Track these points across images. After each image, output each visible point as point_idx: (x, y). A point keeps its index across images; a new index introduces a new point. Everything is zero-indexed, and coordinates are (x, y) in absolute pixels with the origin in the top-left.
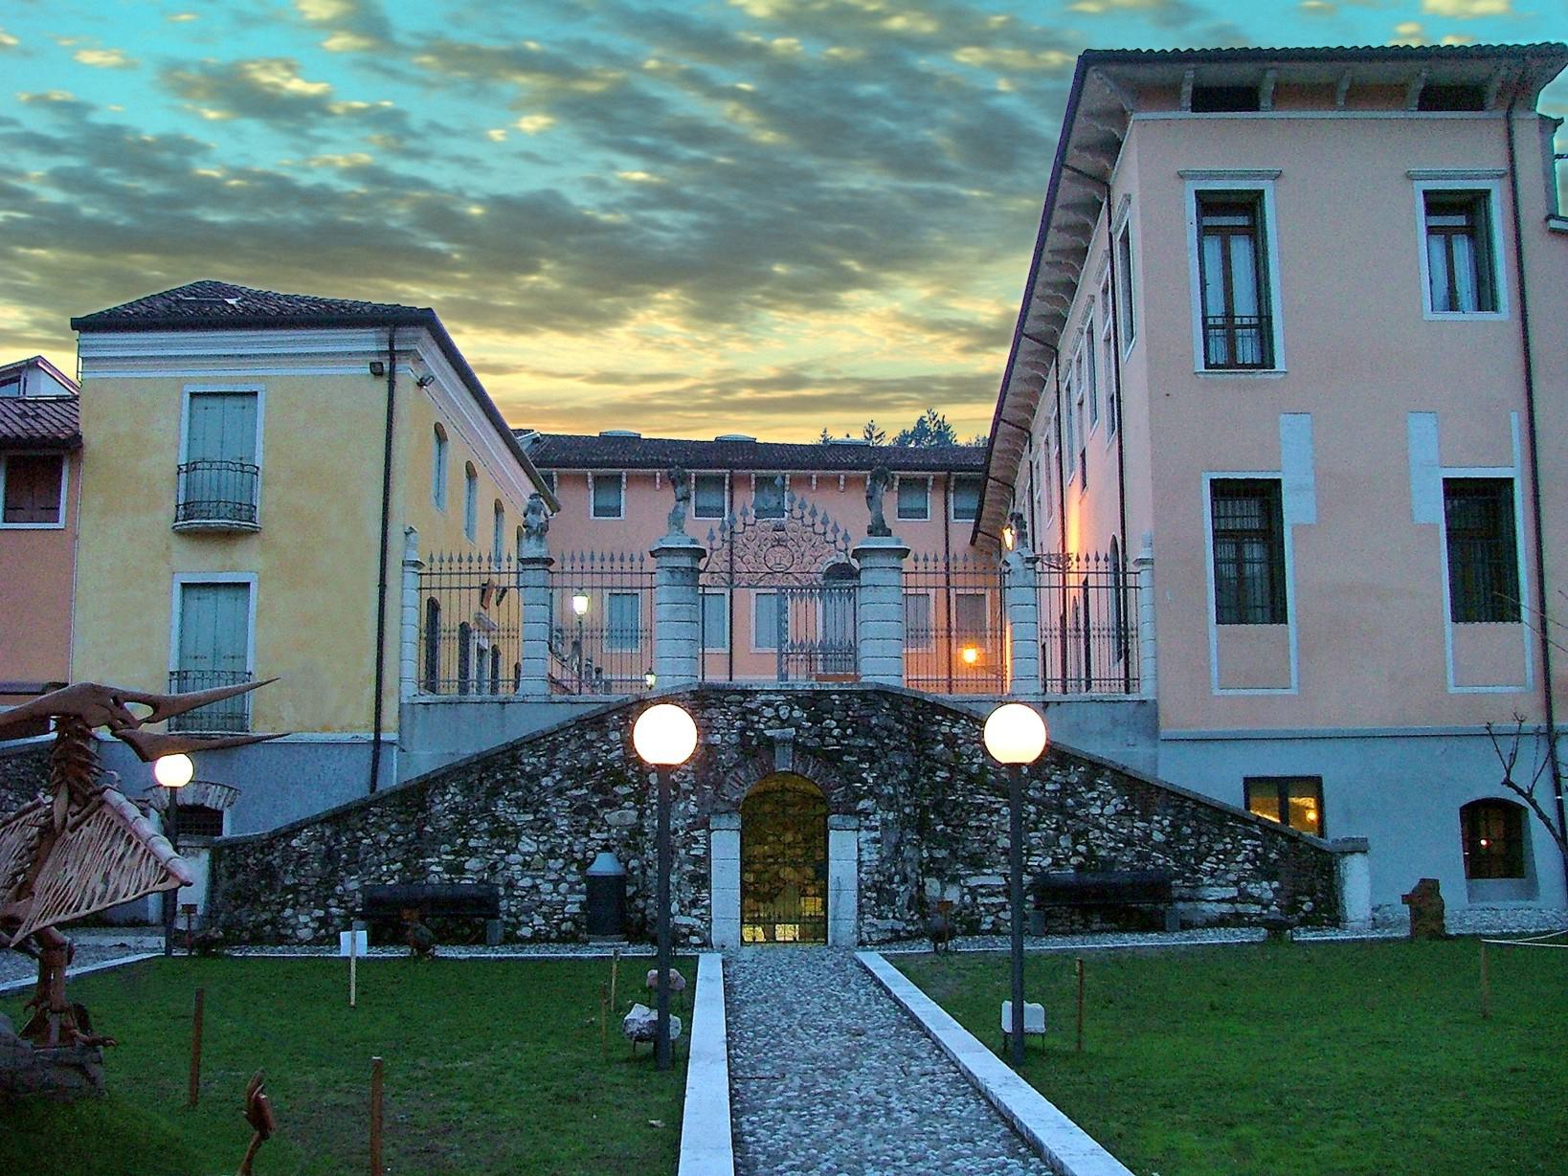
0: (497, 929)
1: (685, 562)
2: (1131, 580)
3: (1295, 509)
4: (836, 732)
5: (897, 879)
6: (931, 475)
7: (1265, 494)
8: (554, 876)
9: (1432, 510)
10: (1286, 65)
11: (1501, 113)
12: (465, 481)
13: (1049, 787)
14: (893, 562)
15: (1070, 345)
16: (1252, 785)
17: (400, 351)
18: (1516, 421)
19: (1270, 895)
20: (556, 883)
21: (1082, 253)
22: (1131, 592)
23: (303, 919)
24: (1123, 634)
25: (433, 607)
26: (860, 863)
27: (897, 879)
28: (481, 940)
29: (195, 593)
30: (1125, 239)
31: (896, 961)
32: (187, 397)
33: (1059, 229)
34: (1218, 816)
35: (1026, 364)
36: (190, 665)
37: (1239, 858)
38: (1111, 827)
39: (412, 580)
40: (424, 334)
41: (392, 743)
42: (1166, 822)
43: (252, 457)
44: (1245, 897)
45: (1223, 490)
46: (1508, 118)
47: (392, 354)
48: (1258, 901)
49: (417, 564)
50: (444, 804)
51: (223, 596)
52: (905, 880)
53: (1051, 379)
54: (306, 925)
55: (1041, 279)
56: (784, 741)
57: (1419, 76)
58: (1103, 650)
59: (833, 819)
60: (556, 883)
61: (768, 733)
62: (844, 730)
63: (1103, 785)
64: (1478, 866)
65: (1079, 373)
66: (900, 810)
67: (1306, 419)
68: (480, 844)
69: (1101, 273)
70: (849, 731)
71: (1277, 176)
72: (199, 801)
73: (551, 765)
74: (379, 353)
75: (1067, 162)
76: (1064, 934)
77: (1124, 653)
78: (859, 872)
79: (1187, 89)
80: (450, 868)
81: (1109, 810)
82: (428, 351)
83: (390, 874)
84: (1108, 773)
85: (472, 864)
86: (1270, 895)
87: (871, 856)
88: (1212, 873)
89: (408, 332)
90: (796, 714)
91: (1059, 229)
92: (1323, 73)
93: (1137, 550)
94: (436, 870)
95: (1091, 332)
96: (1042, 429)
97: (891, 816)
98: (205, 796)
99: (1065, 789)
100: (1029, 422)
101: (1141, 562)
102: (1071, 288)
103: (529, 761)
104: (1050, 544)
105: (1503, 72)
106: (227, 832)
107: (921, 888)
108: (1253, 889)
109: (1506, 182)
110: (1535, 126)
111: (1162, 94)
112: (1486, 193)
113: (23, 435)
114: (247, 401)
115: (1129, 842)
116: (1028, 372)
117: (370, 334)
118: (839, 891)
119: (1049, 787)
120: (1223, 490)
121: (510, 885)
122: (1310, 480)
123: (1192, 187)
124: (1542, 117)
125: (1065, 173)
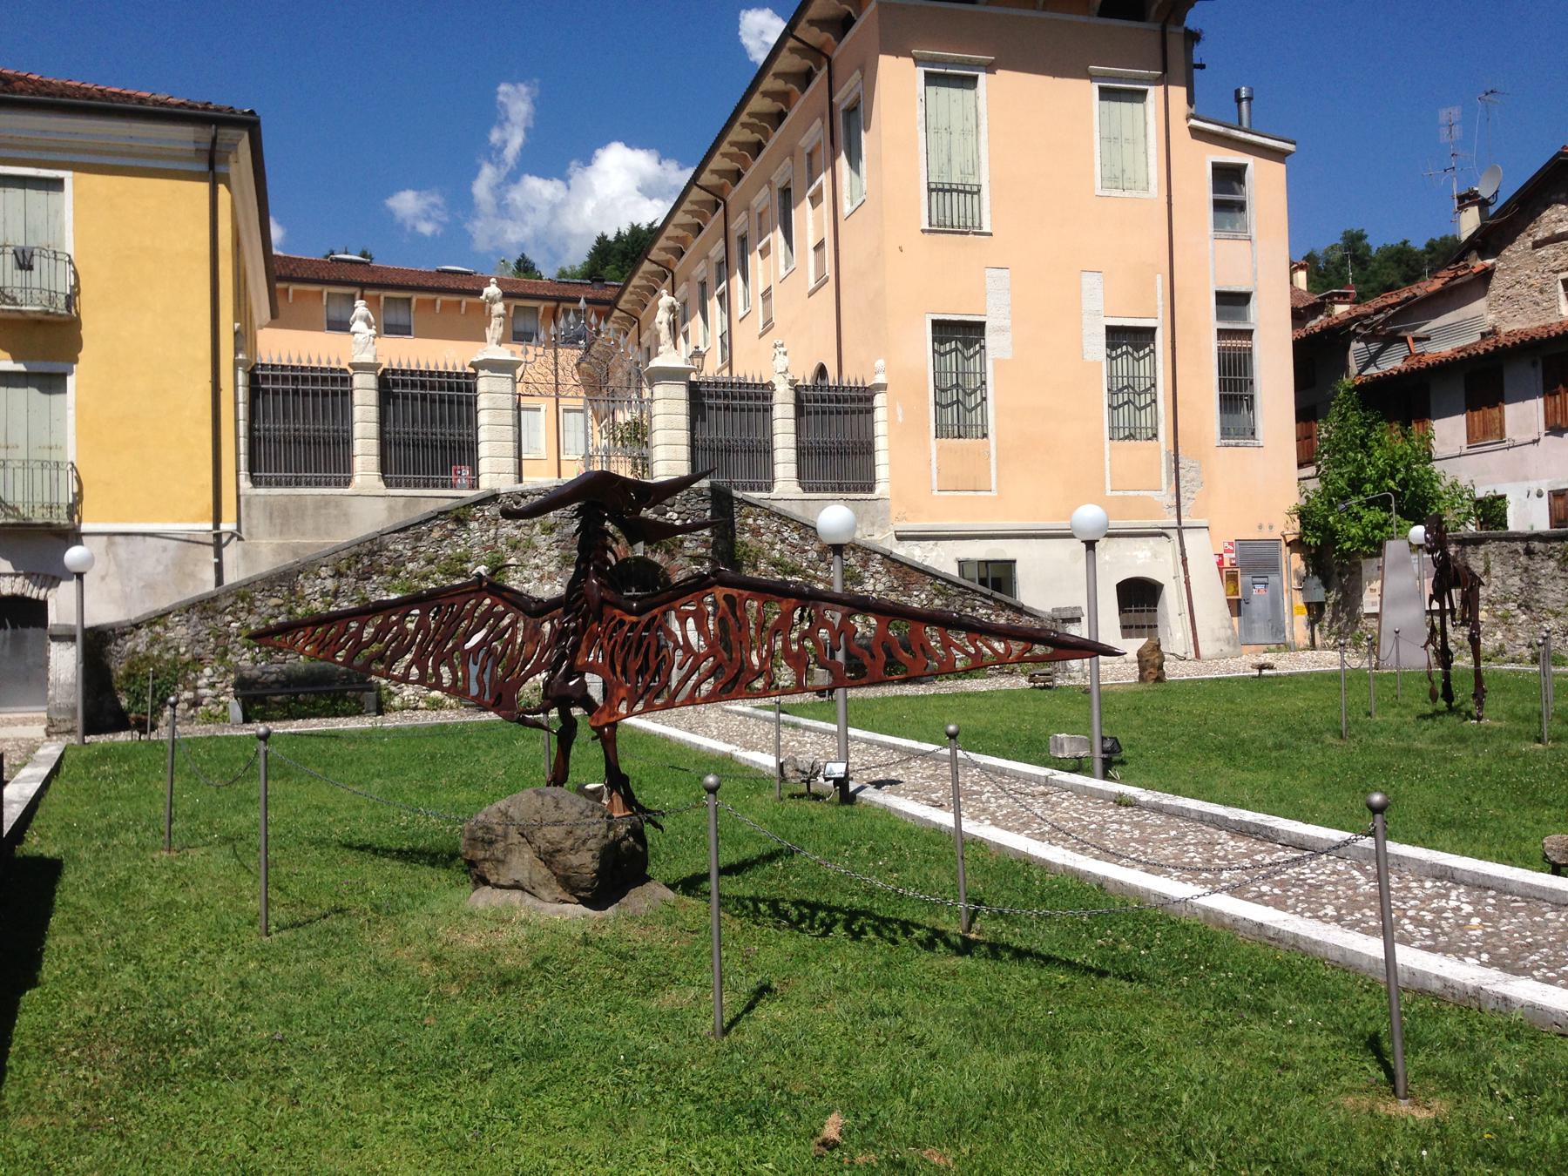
6: (542, 306)
11: (1157, 27)
18: (1161, 282)
122: (1007, 323)
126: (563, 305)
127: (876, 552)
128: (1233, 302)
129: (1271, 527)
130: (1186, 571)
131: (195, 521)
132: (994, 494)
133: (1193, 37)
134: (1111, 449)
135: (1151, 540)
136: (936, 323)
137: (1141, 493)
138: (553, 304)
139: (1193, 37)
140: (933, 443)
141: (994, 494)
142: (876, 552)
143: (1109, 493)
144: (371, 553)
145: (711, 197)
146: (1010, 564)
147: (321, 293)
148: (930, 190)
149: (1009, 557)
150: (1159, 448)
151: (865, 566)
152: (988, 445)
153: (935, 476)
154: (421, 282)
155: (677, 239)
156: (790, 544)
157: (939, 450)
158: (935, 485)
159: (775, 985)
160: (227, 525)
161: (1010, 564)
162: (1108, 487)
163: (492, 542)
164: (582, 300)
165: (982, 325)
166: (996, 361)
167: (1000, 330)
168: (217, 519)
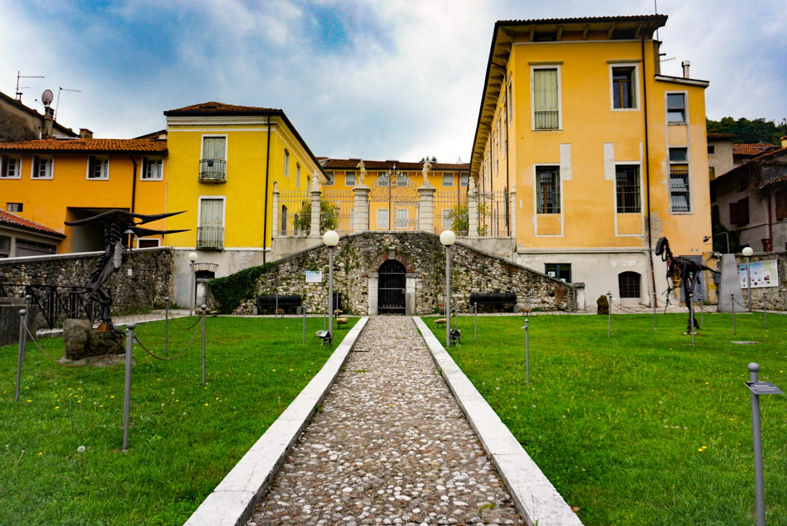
0: (299, 309)
1: (364, 193)
5: (428, 294)
6: (454, 172)
7: (553, 171)
8: (319, 293)
9: (611, 175)
10: (565, 25)
11: (640, 40)
12: (296, 168)
13: (479, 265)
14: (430, 193)
16: (549, 267)
17: (272, 124)
18: (641, 145)
19: (552, 301)
20: (320, 295)
21: (498, 94)
26: (416, 289)
27: (428, 294)
28: (295, 313)
29: (205, 202)
30: (510, 87)
31: (424, 320)
32: (202, 138)
33: (491, 85)
35: (481, 133)
36: (204, 225)
37: (542, 289)
38: (499, 278)
39: (275, 198)
40: (280, 118)
41: (269, 251)
42: (517, 277)
43: (224, 158)
45: (540, 170)
46: (643, 42)
48: (548, 303)
49: (278, 193)
50: (285, 268)
51: (215, 202)
53: (489, 138)
55: (485, 103)
57: (613, 27)
60: (320, 295)
62: (412, 246)
63: (497, 265)
64: (624, 294)
65: (501, 139)
66: (430, 272)
67: (569, 145)
70: (413, 246)
71: (561, 63)
72: (207, 269)
73: (318, 257)
76: (17, 117)
79: (532, 34)
80: (286, 290)
81: (499, 273)
82: (281, 124)
84: (498, 261)
86: (552, 301)
90: (396, 241)
91: (491, 85)
92: (579, 27)
93: (512, 190)
95: (500, 120)
96: (487, 155)
98: (209, 267)
100: (483, 153)
101: (513, 193)
102: (495, 106)
103: (312, 256)
104: (488, 189)
105: (641, 25)
106: (216, 277)
108: (546, 299)
109: (641, 64)
110: (652, 44)
111: (524, 36)
112: (634, 68)
113: (149, 150)
114: (222, 140)
116: (483, 135)
117: (261, 118)
120: (540, 170)
122: (570, 166)
124: (654, 41)
125: (492, 65)
127: (497, 259)
128: (678, 153)
129: (697, 250)
130: (652, 269)
132: (562, 236)
133: (658, 43)
134: (618, 217)
135: (636, 256)
137: (632, 235)
138: (458, 171)
139: (658, 43)
140: (536, 216)
141: (32, 177)
142: (497, 259)
146: (569, 265)
147: (343, 172)
148: (536, 113)
149: (568, 262)
150: (641, 216)
151: (492, 264)
152: (560, 217)
154: (442, 167)
155: (482, 143)
156: (461, 256)
157: (538, 219)
161: (569, 265)
164: (40, 138)
165: (558, 168)
167: (566, 169)
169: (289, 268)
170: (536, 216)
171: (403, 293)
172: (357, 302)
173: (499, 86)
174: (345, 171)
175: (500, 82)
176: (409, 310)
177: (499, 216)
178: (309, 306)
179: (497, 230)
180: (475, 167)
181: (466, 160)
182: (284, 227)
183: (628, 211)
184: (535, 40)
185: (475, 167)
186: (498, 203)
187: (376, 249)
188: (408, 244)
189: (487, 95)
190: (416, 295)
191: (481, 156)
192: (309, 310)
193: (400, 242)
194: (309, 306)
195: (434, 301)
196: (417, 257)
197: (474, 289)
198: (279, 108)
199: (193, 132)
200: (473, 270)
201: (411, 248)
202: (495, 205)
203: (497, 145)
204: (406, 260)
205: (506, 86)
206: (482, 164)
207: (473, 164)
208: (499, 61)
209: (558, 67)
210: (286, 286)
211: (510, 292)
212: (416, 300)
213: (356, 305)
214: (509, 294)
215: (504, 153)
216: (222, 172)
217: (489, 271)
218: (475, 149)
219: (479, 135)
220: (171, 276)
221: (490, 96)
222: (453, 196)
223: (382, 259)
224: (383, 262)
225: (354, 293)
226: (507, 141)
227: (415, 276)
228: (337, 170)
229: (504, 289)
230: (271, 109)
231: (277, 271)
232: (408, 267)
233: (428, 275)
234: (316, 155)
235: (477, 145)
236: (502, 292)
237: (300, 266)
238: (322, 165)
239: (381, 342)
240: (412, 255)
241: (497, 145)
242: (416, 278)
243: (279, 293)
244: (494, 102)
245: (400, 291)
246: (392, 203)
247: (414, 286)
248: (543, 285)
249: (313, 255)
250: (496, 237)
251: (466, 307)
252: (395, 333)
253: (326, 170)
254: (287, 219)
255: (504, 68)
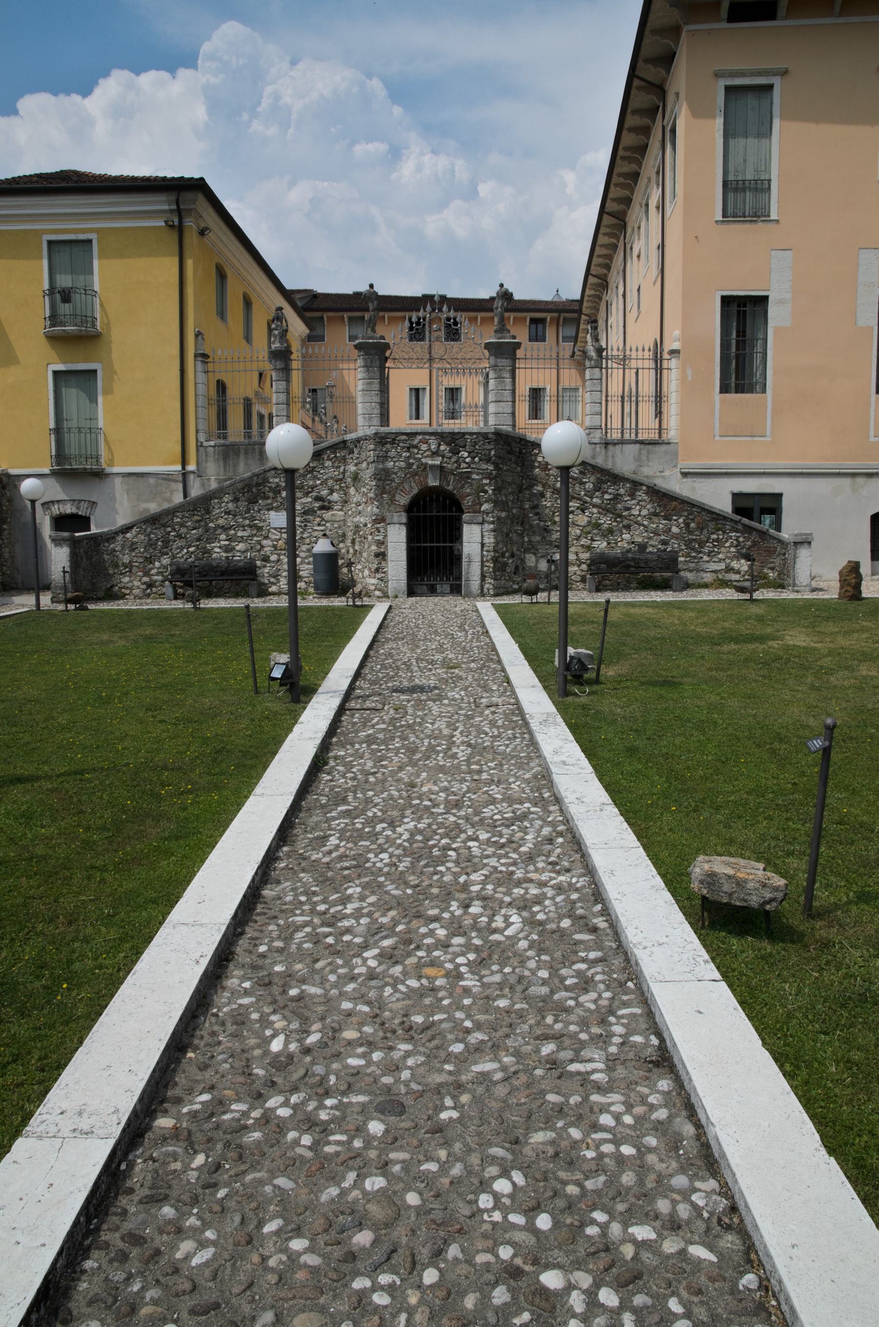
2: (665, 364)
3: (777, 316)
4: (468, 460)
6: (548, 316)
13: (607, 496)
15: (635, 215)
22: (665, 372)
23: (136, 583)
24: (659, 399)
25: (221, 387)
26: (483, 545)
27: (507, 555)
30: (673, 131)
32: (45, 245)
34: (716, 517)
35: (605, 234)
37: (727, 544)
38: (646, 523)
41: (193, 472)
42: (681, 520)
44: (729, 569)
47: (179, 212)
52: (513, 556)
54: (138, 587)
56: (432, 466)
58: (647, 410)
59: (465, 517)
61: (424, 460)
62: (473, 458)
63: (641, 494)
65: (647, 244)
68: (245, 534)
69: (656, 158)
70: (477, 459)
71: (784, 73)
74: (171, 211)
75: (637, 73)
77: (659, 413)
78: (482, 550)
80: (227, 549)
81: (644, 512)
83: (185, 554)
85: (241, 547)
87: (490, 540)
88: (709, 554)
89: (188, 195)
93: (671, 344)
94: (217, 553)
96: (614, 277)
97: (503, 514)
99: (617, 498)
100: (606, 275)
107: (523, 561)
108: (735, 564)
115: (656, 533)
118: (470, 562)
119: (607, 496)
121: (266, 559)
123: (722, 83)
125: (636, 82)
126: (563, 315)
131: (165, 464)
132: (768, 439)
136: (723, 298)
138: (556, 315)
141: (768, 439)
143: (872, 439)
144: (258, 485)
145: (618, 221)
146: (778, 496)
147: (343, 318)
149: (777, 490)
151: (632, 495)
153: (717, 425)
158: (717, 431)
159: (829, 721)
160: (191, 467)
161: (778, 496)
162: (872, 433)
163: (341, 476)
166: (776, 329)
167: (782, 302)
168: (184, 463)
169: (231, 506)
170: (717, 397)
171: (456, 553)
172: (366, 572)
173: (646, 131)
174: (346, 315)
175: (649, 121)
176: (468, 587)
177: (640, 399)
178: (272, 580)
179: (633, 426)
180: (590, 304)
181: (572, 290)
182: (222, 423)
183: (740, 389)
184: (734, 17)
185: (590, 304)
186: (637, 374)
187: (403, 464)
188: (466, 454)
189: (621, 153)
190: (482, 556)
191: (604, 284)
192: (273, 589)
193: (450, 451)
194: (272, 580)
195: (517, 567)
196: (485, 481)
197: (595, 544)
198: (197, 176)
199: (24, 231)
200: (594, 506)
201: (473, 462)
202: (631, 375)
203: (639, 256)
204: (463, 487)
205: (663, 127)
206: (605, 298)
207: (586, 298)
208: (650, 73)
209: (776, 81)
210: (227, 543)
211: (665, 550)
212: (482, 566)
213: (365, 578)
214: (663, 555)
215: (655, 271)
216: (89, 314)
217: (629, 509)
218: (592, 267)
219: (602, 240)
220: (5, 526)
221: (628, 154)
222: (548, 356)
223: (413, 485)
224: (415, 491)
225: (361, 553)
226: (662, 247)
227: (480, 519)
228: (331, 314)
229: (654, 546)
230: (182, 178)
231: (208, 512)
232: (467, 502)
233: (507, 517)
234: (289, 285)
235: (595, 260)
236: (650, 549)
237: (253, 501)
238: (299, 304)
239: (411, 679)
240: (474, 476)
241: (639, 256)
242: (482, 523)
243: (214, 555)
244: (634, 167)
245: (451, 547)
246: (434, 371)
247: (479, 539)
248: (731, 537)
249: (277, 480)
250: (633, 437)
251: (579, 578)
252: (440, 649)
253: (309, 314)
254: (230, 410)
255: (660, 90)
